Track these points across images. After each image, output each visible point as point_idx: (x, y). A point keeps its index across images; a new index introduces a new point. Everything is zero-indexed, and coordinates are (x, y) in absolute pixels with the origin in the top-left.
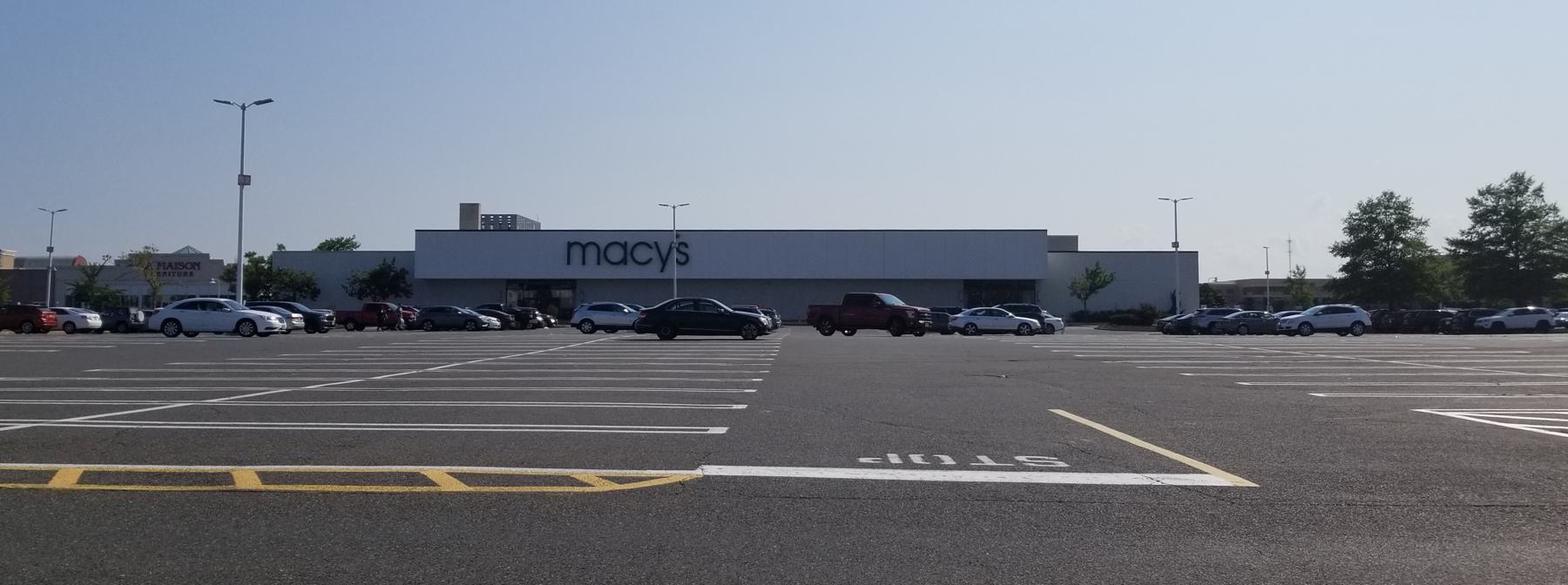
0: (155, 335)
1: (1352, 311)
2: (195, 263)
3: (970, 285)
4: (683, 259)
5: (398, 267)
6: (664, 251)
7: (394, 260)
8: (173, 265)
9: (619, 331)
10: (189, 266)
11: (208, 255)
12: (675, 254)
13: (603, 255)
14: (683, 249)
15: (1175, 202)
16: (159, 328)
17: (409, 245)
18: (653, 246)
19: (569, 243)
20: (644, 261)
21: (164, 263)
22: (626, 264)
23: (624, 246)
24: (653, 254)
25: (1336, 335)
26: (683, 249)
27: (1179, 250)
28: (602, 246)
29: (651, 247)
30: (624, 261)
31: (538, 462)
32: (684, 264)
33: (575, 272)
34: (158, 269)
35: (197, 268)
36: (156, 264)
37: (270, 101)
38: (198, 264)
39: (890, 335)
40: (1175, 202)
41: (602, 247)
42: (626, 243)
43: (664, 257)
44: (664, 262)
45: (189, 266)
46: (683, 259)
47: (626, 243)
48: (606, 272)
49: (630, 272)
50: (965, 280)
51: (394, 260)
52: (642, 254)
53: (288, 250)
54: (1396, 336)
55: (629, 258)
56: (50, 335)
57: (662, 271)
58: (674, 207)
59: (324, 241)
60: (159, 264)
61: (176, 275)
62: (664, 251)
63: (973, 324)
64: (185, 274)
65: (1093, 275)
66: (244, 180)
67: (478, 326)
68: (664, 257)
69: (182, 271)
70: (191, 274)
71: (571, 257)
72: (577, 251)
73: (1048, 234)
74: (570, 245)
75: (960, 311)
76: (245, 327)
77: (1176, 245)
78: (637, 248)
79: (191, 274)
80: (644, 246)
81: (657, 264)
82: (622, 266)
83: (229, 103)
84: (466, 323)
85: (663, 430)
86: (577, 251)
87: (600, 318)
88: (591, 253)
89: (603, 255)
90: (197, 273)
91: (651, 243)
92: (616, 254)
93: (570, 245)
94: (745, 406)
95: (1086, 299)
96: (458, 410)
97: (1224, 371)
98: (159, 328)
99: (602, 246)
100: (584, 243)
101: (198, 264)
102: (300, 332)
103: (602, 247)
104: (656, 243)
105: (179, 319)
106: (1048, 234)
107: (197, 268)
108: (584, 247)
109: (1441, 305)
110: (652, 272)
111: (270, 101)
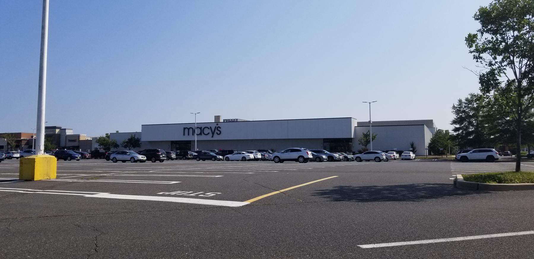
1: (300, 151)
3: (326, 140)
4: (219, 132)
5: (136, 137)
6: (213, 130)
7: (135, 135)
11: (78, 136)
12: (216, 131)
14: (219, 129)
15: (370, 103)
16: (374, 159)
17: (139, 130)
18: (210, 128)
23: (201, 128)
24: (209, 131)
25: (63, 160)
26: (219, 129)
29: (209, 128)
31: (46, 189)
39: (106, 160)
40: (370, 103)
42: (201, 127)
43: (213, 131)
44: (213, 134)
46: (219, 132)
50: (324, 139)
51: (135, 135)
52: (206, 131)
53: (119, 132)
56: (4, 164)
57: (212, 137)
62: (213, 130)
63: (278, 157)
67: (215, 159)
68: (213, 131)
72: (186, 131)
74: (185, 129)
78: (205, 129)
80: (207, 128)
81: (211, 135)
82: (200, 135)
86: (186, 131)
87: (119, 157)
92: (197, 131)
93: (185, 129)
94: (450, 179)
98: (374, 159)
100: (189, 128)
102: (365, 159)
104: (211, 127)
108: (189, 129)
110: (209, 138)
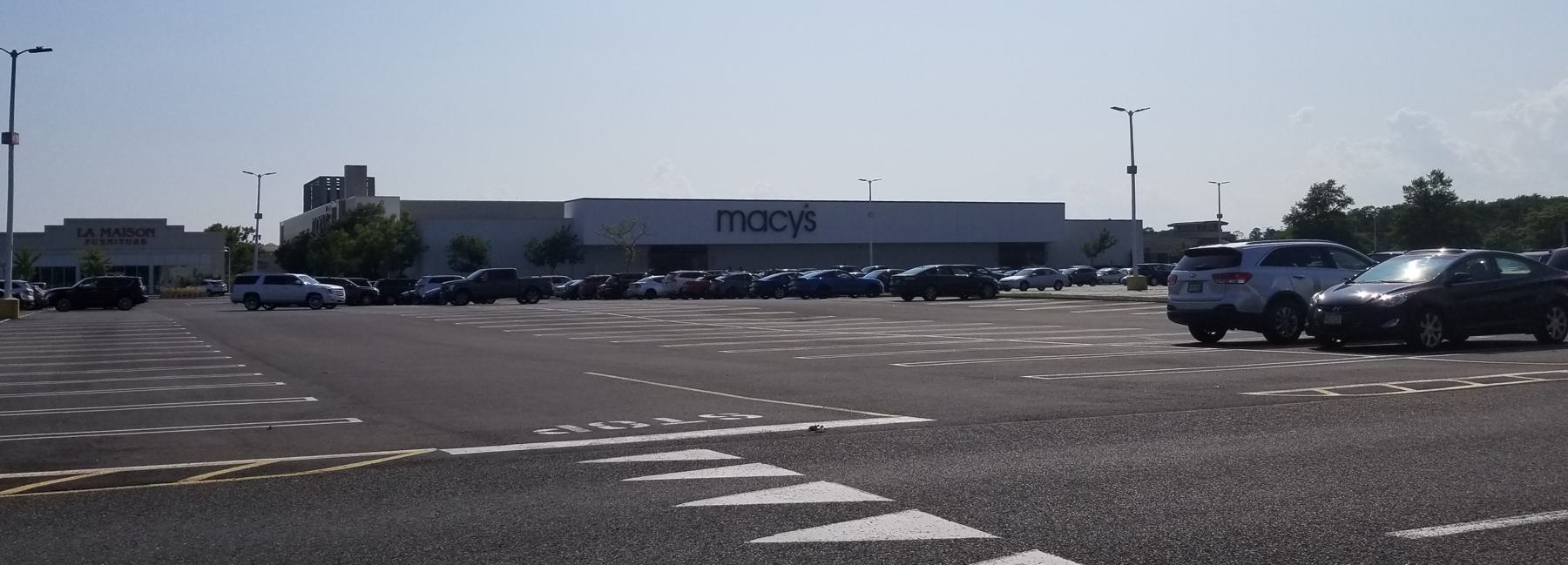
0: (198, 301)
6: (796, 220)
8: (121, 231)
13: (746, 223)
18: (787, 213)
19: (719, 211)
20: (781, 227)
21: (109, 230)
22: (766, 230)
23: (764, 214)
24: (786, 221)
27: (1222, 220)
28: (747, 214)
29: (786, 216)
30: (764, 228)
32: (811, 230)
33: (725, 238)
34: (102, 235)
35: (150, 234)
37: (50, 50)
38: (153, 231)
41: (747, 215)
44: (796, 228)
45: (141, 233)
46: (810, 226)
47: (766, 212)
48: (749, 238)
49: (768, 238)
52: (779, 222)
54: (839, 299)
55: (768, 226)
60: (103, 230)
61: (124, 242)
65: (1104, 238)
66: (1132, 170)
69: (133, 238)
70: (144, 242)
71: (722, 222)
72: (725, 220)
74: (720, 213)
75: (641, 277)
77: (1220, 216)
79: (144, 242)
81: (790, 230)
83: (31, 51)
86: (725, 220)
88: (738, 220)
89: (746, 223)
91: (785, 211)
92: (757, 222)
93: (720, 213)
95: (1095, 255)
99: (747, 214)
101: (153, 231)
103: (747, 215)
107: (150, 234)
108: (732, 215)
109: (22, 276)
110: (785, 238)
111: (50, 50)
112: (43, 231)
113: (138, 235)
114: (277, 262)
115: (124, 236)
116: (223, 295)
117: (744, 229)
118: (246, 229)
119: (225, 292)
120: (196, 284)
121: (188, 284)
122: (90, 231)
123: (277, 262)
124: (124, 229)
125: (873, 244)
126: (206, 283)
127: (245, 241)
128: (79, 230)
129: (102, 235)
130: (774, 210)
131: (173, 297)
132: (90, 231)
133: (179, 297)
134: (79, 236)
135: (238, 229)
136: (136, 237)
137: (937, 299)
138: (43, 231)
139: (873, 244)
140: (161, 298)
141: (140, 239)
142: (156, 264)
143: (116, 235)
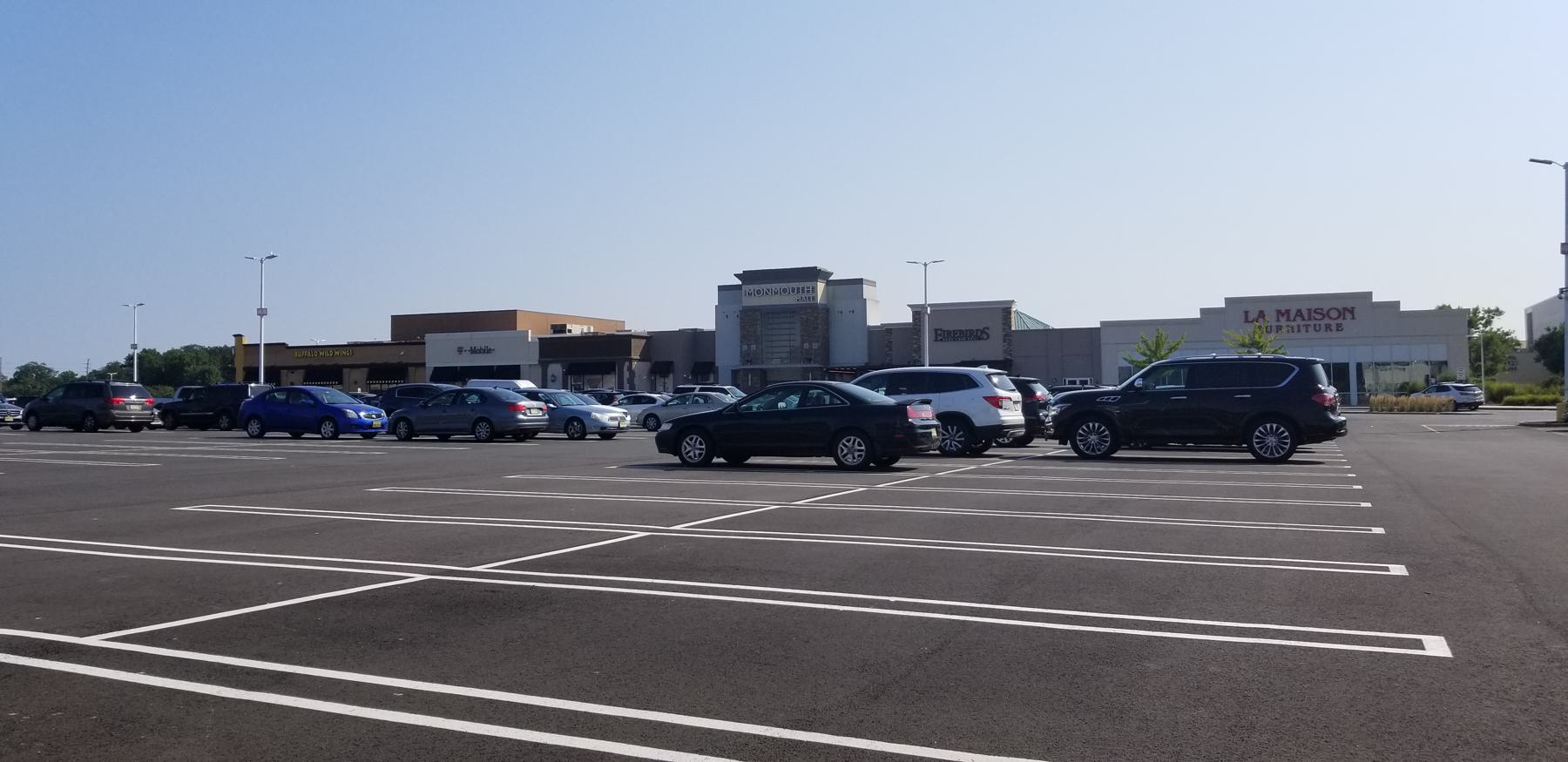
2: (1345, 309)
9: (112, 429)
10: (1334, 314)
11: (1370, 294)
21: (1288, 312)
34: (1278, 320)
35: (1348, 315)
36: (1275, 314)
38: (1352, 311)
45: (1334, 314)
58: (925, 265)
59: (170, 349)
60: (1279, 312)
64: (1328, 327)
69: (1323, 323)
70: (1339, 328)
73: (1402, 309)
76: (574, 426)
79: (1339, 328)
84: (321, 421)
85: (1122, 555)
90: (1347, 323)
96: (888, 517)
97: (48, 448)
101: (1352, 311)
105: (657, 414)
106: (1402, 309)
107: (1348, 315)
112: (1198, 316)
113: (1330, 318)
114: (1538, 360)
115: (1310, 319)
116: (1476, 408)
117: (1326, 330)
118: (1489, 311)
119: (1481, 403)
120: (1427, 391)
121: (1413, 390)
122: (1262, 314)
123: (1538, 360)
124: (1309, 310)
125: (265, 345)
126: (1446, 389)
127: (1488, 329)
128: (1246, 313)
129: (1278, 320)
130: (1329, 308)
131: (1391, 411)
132: (1262, 314)
133: (1402, 410)
134: (1247, 321)
135: (1476, 311)
136: (1326, 321)
137: (753, 460)
138: (1198, 316)
139: (265, 345)
140: (1371, 411)
141: (1333, 323)
142: (461, 346)
143: (1299, 319)
